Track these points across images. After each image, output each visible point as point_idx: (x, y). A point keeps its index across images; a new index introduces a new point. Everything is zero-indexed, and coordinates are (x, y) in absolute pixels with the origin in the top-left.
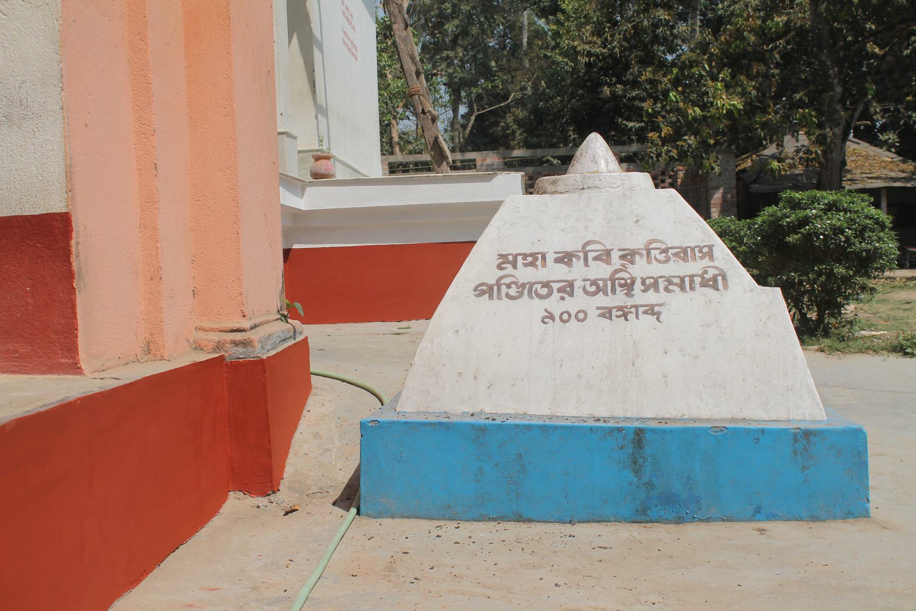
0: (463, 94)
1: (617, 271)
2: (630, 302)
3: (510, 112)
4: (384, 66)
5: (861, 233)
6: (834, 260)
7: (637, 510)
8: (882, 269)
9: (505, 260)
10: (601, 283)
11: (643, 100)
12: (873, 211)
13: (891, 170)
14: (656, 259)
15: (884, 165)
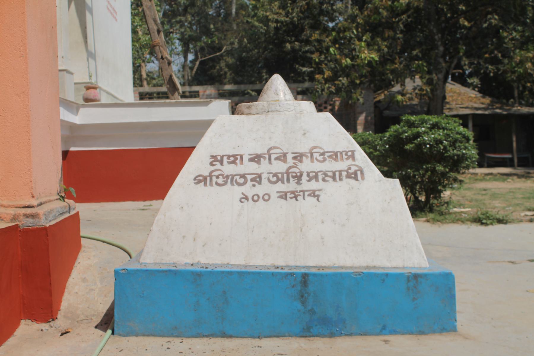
0: (191, 46)
1: (290, 167)
2: (299, 188)
3: (223, 59)
4: (137, 26)
5: (453, 144)
6: (436, 161)
7: (304, 329)
8: (467, 167)
9: (215, 159)
10: (280, 175)
11: (312, 53)
12: (461, 129)
13: (475, 103)
14: (317, 159)
15: (471, 99)
